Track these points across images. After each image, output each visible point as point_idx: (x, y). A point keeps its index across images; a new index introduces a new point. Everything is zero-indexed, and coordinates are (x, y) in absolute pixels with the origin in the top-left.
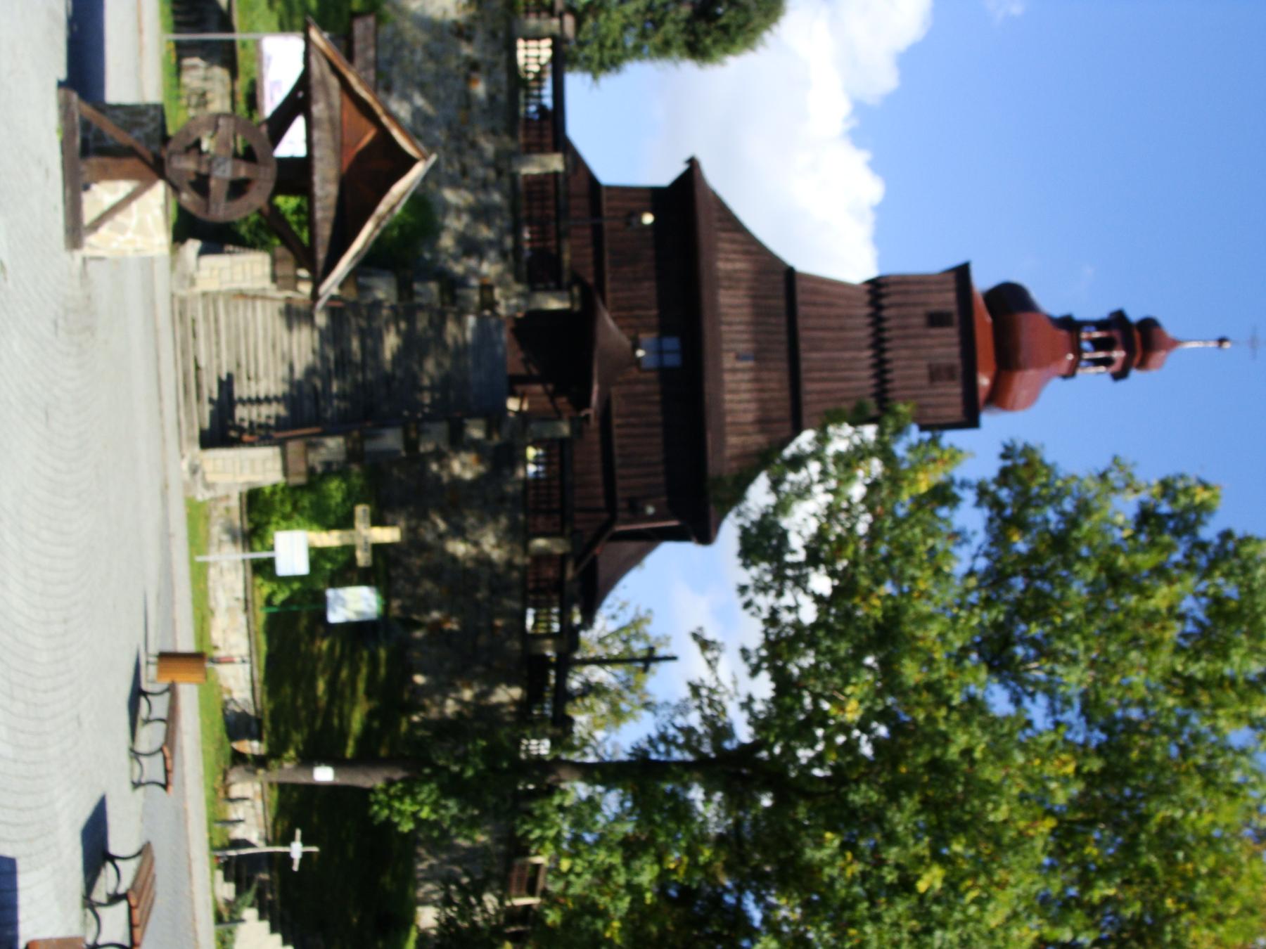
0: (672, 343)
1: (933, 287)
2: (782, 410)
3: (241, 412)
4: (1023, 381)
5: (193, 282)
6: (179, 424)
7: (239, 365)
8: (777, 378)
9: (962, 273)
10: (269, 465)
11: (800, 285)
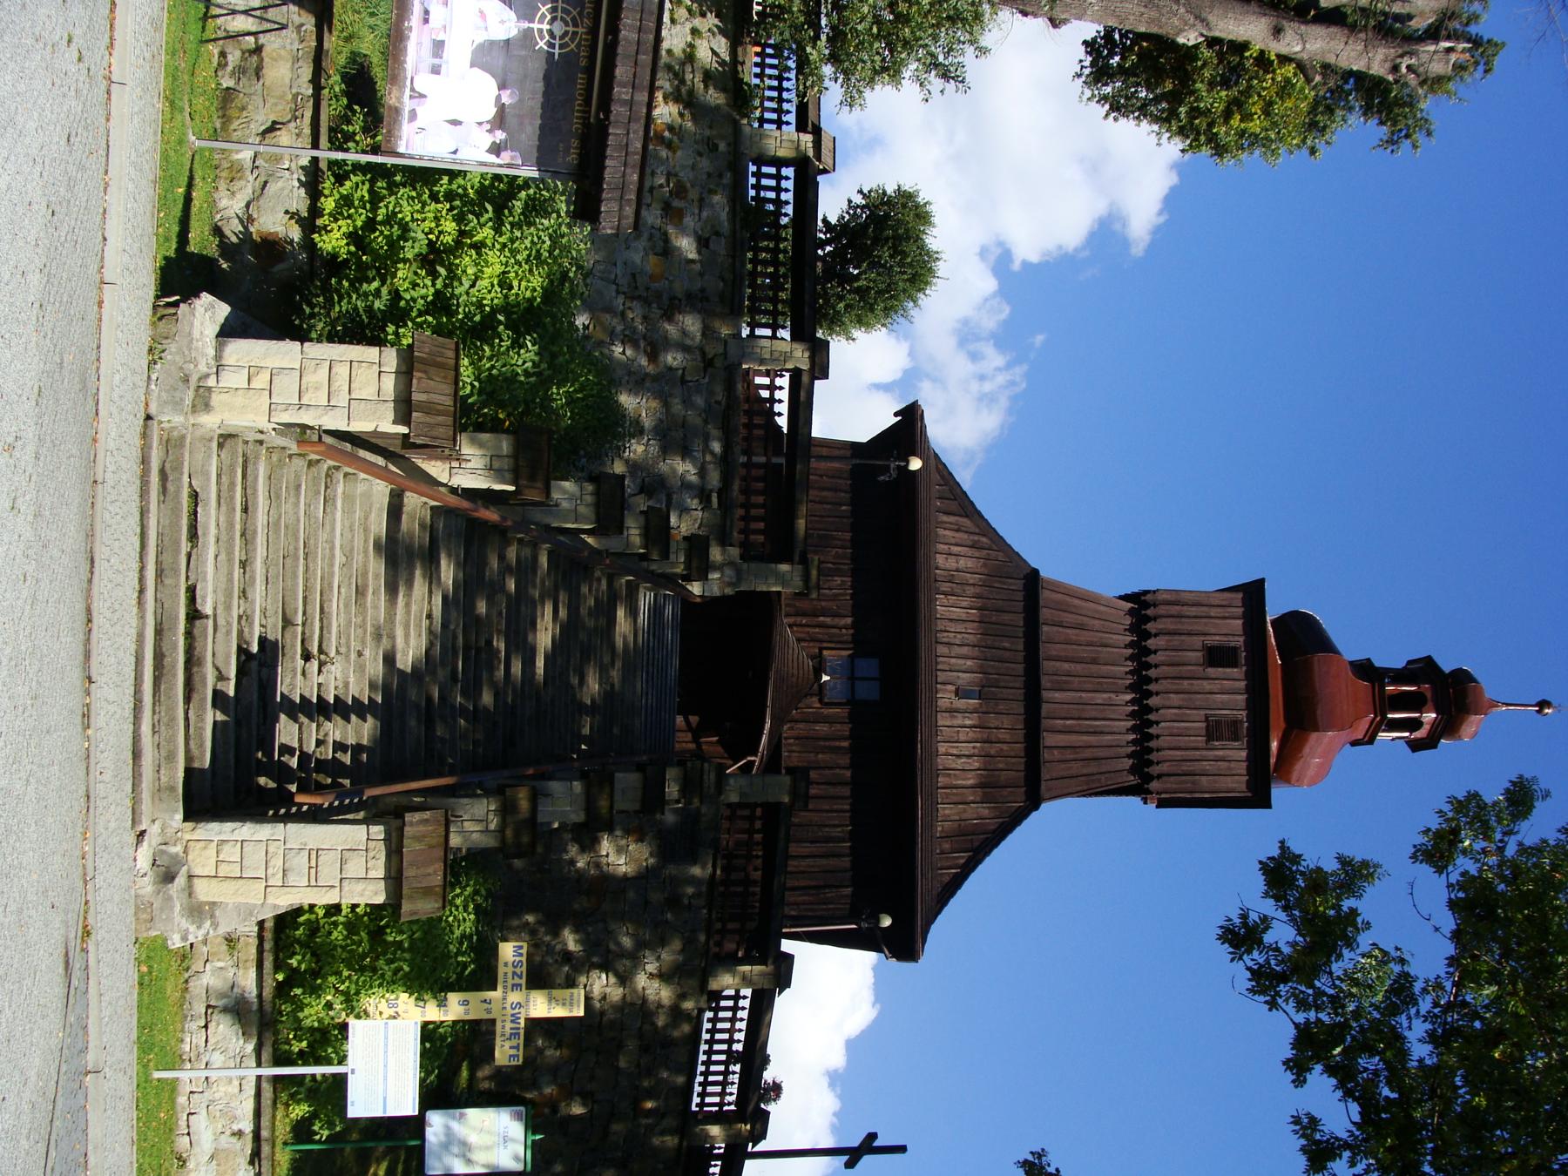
0: (869, 667)
1: (1213, 612)
2: (1013, 769)
3: (286, 731)
4: (1319, 746)
5: (203, 401)
6: (136, 755)
7: (287, 622)
8: (1009, 725)
9: (1253, 593)
10: (355, 867)
11: (1045, 595)
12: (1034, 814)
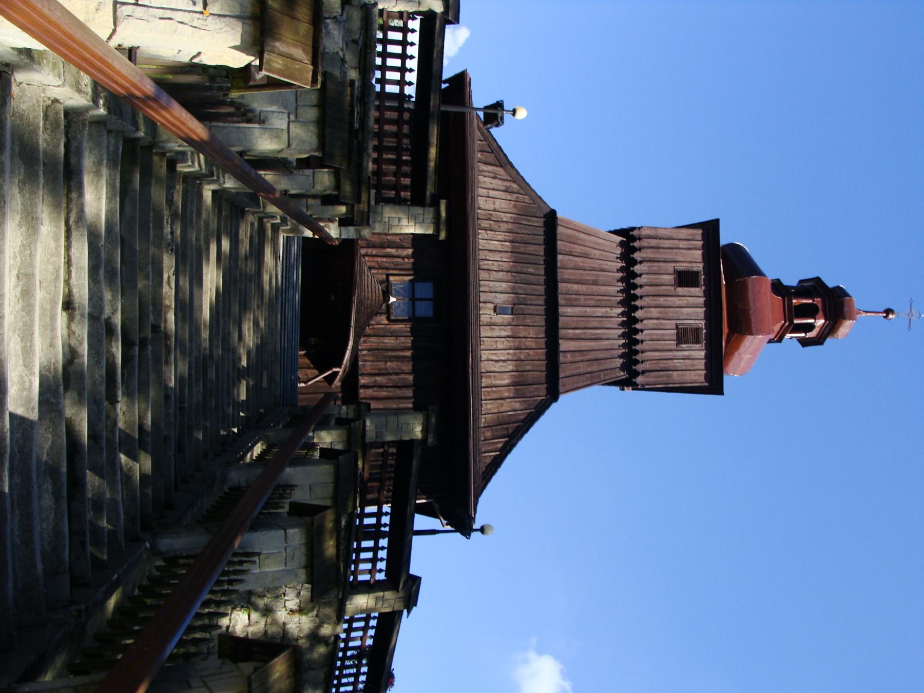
12: (554, 405)
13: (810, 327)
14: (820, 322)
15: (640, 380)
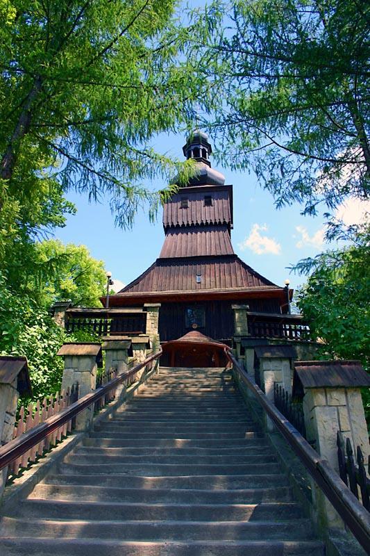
12: (238, 257)
13: (203, 150)
14: (202, 147)
15: (227, 221)
